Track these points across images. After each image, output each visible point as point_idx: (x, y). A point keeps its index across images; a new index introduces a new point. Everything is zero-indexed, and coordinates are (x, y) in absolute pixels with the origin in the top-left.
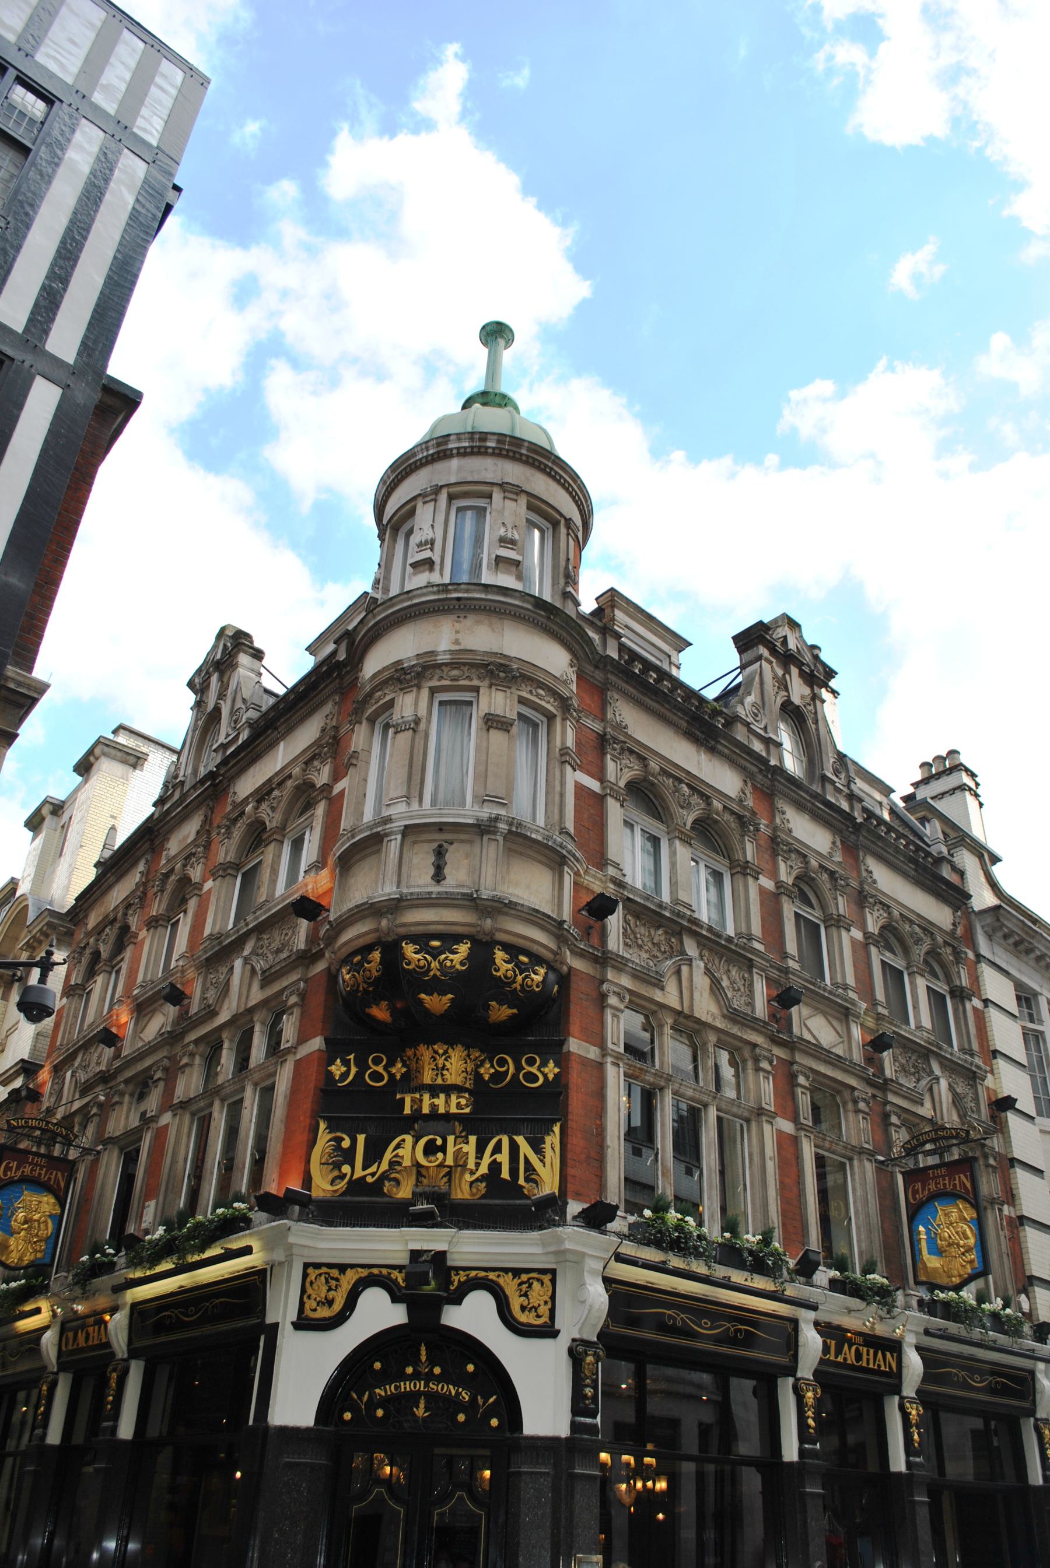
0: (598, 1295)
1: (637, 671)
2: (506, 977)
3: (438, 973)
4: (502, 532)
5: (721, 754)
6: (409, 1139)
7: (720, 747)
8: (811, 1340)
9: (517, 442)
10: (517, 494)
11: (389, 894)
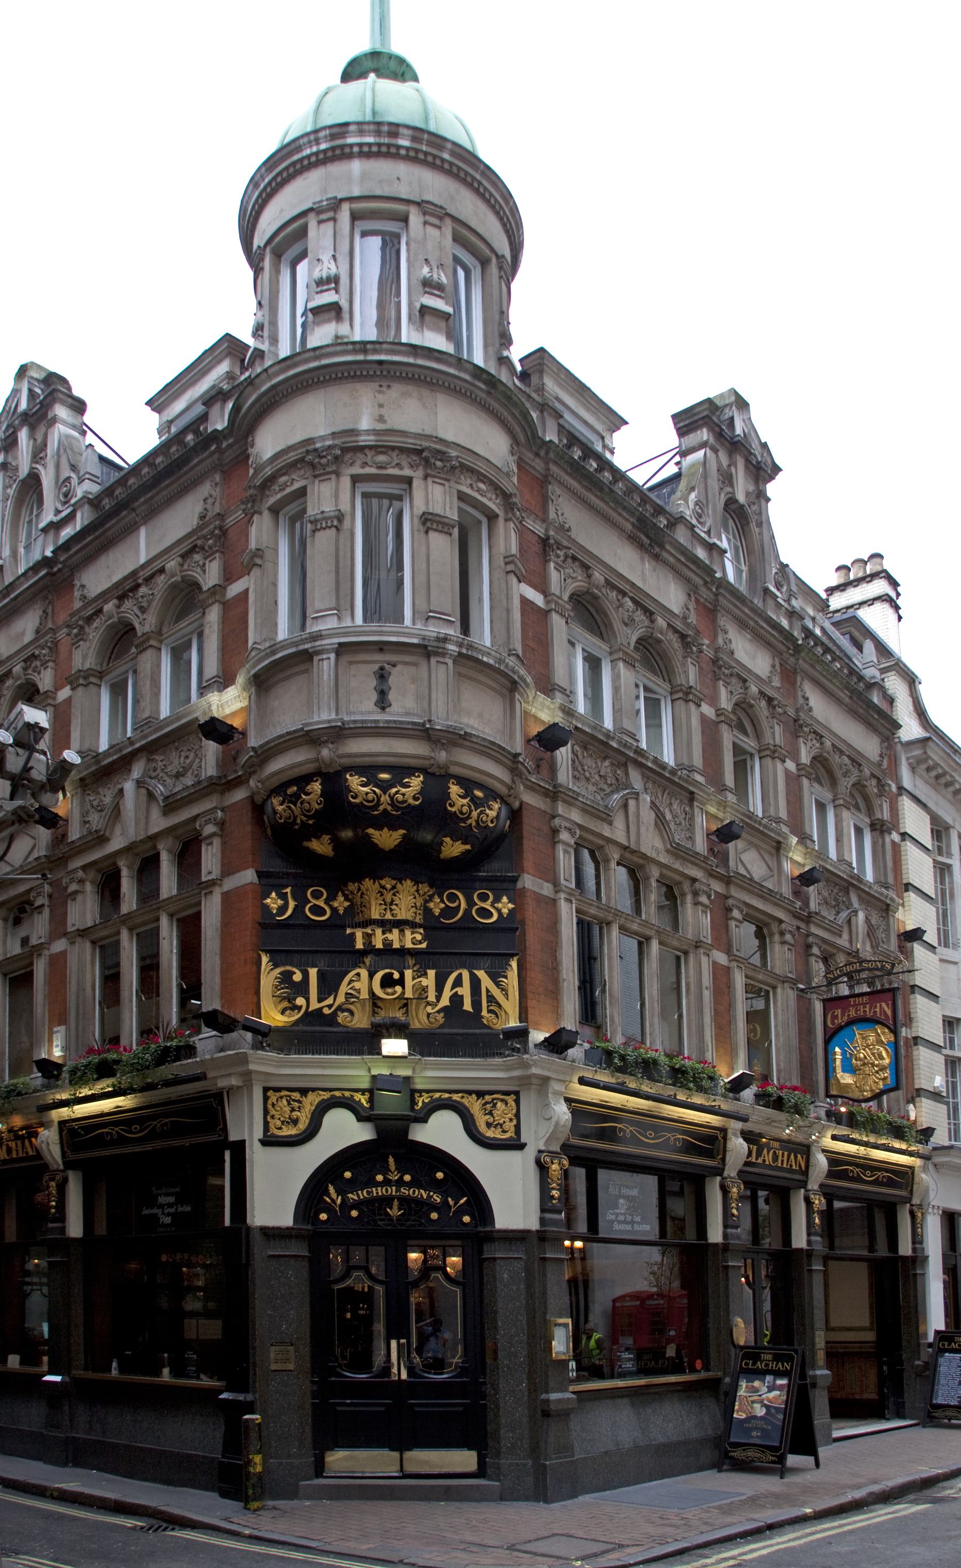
0: (562, 1111)
1: (576, 458)
2: (461, 813)
3: (389, 808)
4: (425, 270)
5: (665, 563)
6: (364, 973)
7: (665, 554)
8: (738, 1146)
9: (438, 140)
10: (441, 218)
11: (329, 721)
